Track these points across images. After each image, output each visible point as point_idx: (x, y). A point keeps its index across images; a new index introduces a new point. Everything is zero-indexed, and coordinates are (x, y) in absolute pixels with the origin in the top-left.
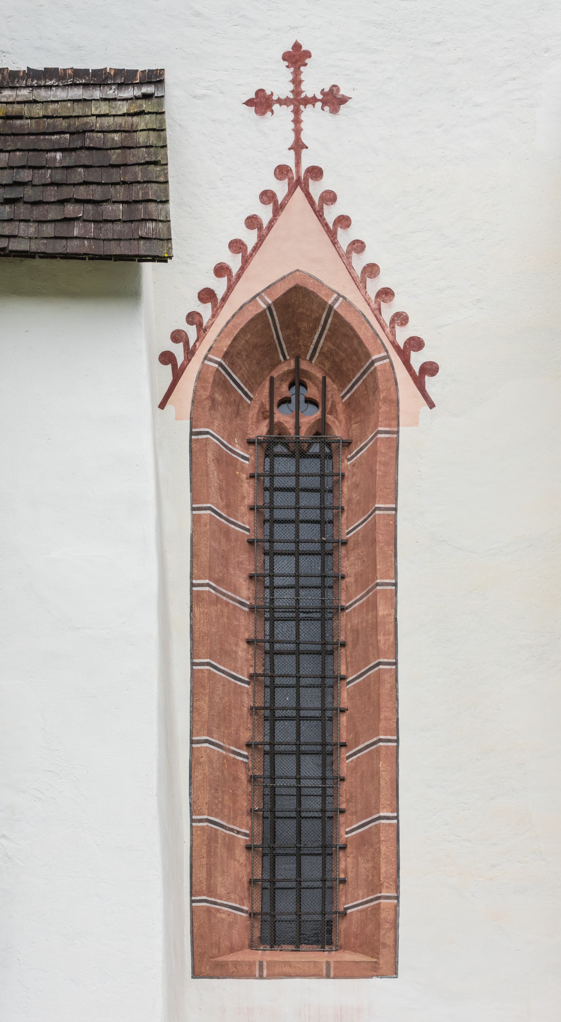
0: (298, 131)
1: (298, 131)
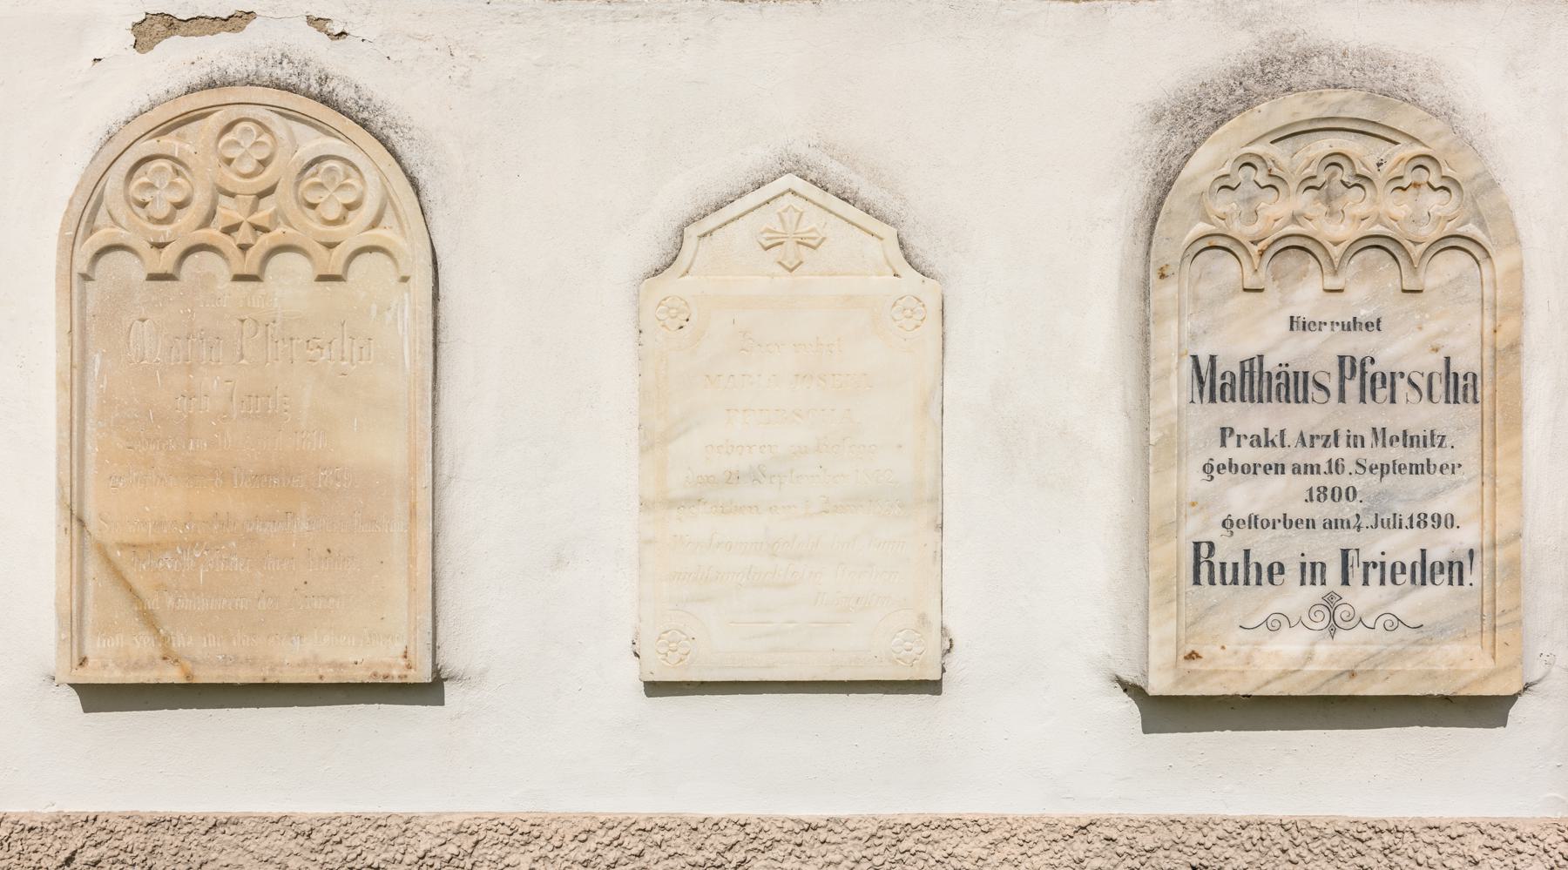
0: (801, 196)
1: (801, 196)
